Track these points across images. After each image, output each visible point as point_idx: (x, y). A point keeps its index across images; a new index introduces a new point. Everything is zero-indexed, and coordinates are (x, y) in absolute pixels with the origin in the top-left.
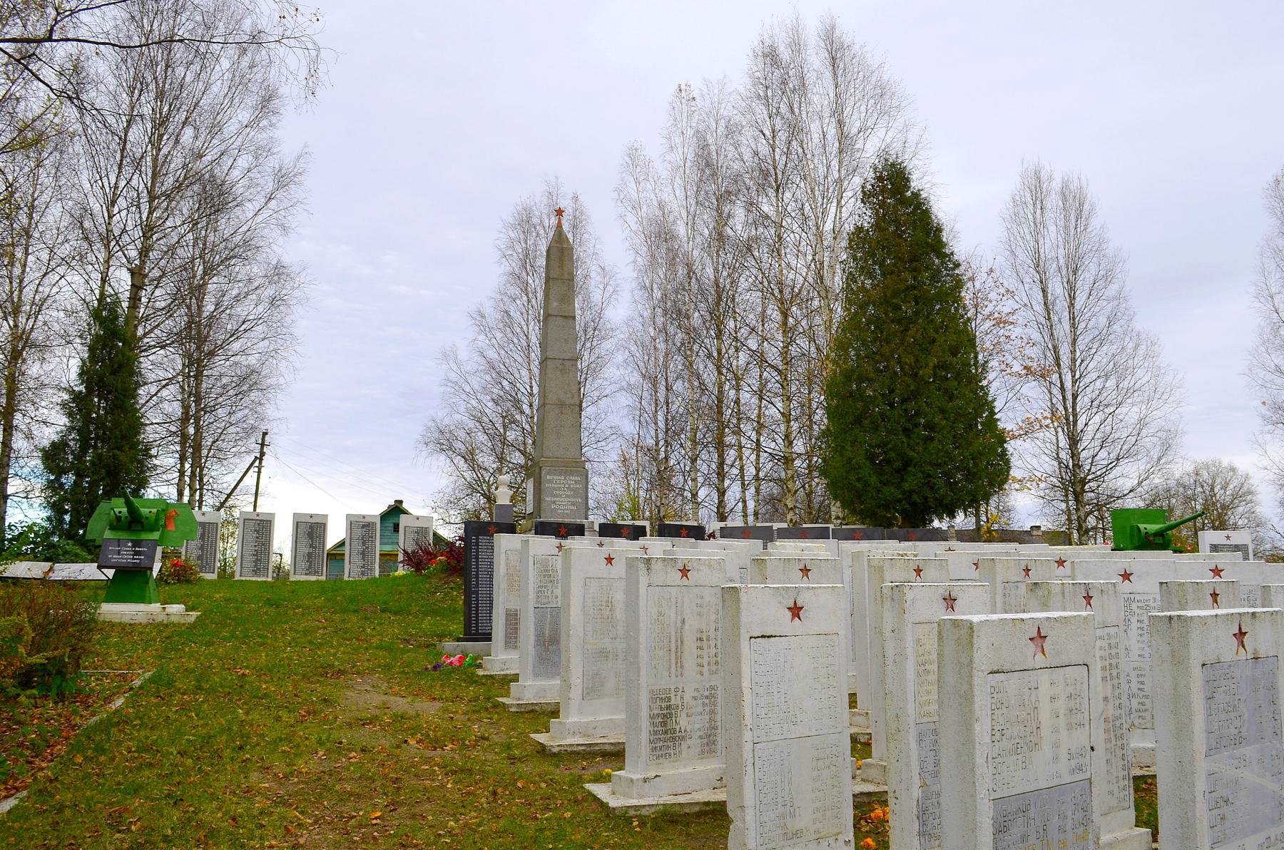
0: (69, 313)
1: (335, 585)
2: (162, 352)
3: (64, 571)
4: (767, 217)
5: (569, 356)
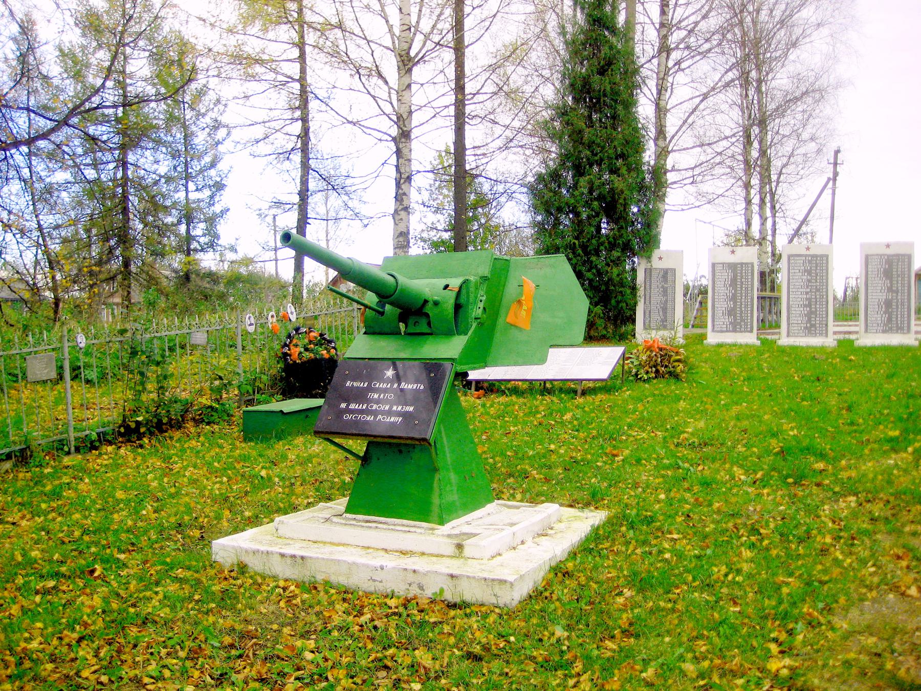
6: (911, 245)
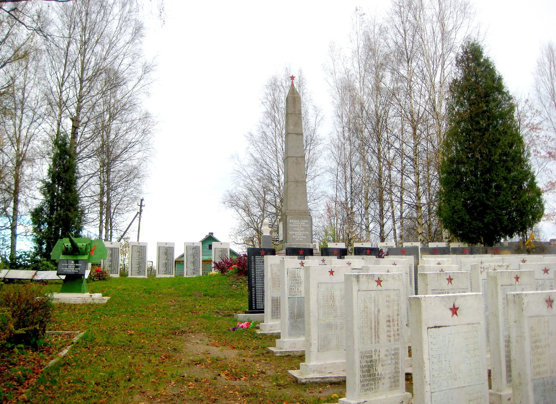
0: (45, 142)
1: (179, 280)
2: (90, 160)
3: (43, 275)
4: (403, 77)
5: (300, 155)
6: (174, 244)
